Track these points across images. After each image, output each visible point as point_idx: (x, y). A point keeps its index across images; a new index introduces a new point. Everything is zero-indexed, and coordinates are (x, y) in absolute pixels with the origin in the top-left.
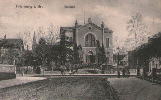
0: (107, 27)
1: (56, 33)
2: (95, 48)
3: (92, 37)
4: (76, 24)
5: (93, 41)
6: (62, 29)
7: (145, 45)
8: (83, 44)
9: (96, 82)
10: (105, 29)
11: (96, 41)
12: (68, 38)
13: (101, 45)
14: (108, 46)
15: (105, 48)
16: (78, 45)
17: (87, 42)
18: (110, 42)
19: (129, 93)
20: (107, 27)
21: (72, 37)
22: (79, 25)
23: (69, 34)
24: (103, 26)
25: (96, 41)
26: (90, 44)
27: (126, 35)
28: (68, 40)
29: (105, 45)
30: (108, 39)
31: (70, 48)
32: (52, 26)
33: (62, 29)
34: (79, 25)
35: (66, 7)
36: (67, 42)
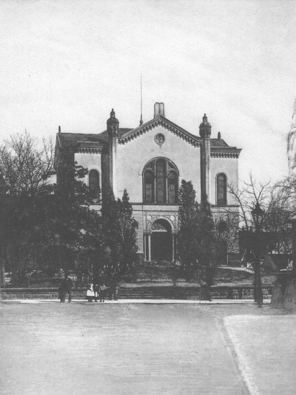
1: (44, 149)
2: (176, 208)
3: (168, 169)
4: (112, 122)
9: (187, 377)
10: (213, 141)
11: (180, 184)
12: (83, 172)
13: (198, 199)
14: (222, 202)
15: (213, 210)
16: (118, 195)
17: (148, 186)
18: (228, 189)
19: (128, 357)
21: (99, 169)
23: (88, 160)
24: (205, 128)
25: (180, 184)
26: (161, 193)
28: (86, 180)
29: (212, 199)
30: (221, 178)
31: (91, 207)
35: (60, 127)
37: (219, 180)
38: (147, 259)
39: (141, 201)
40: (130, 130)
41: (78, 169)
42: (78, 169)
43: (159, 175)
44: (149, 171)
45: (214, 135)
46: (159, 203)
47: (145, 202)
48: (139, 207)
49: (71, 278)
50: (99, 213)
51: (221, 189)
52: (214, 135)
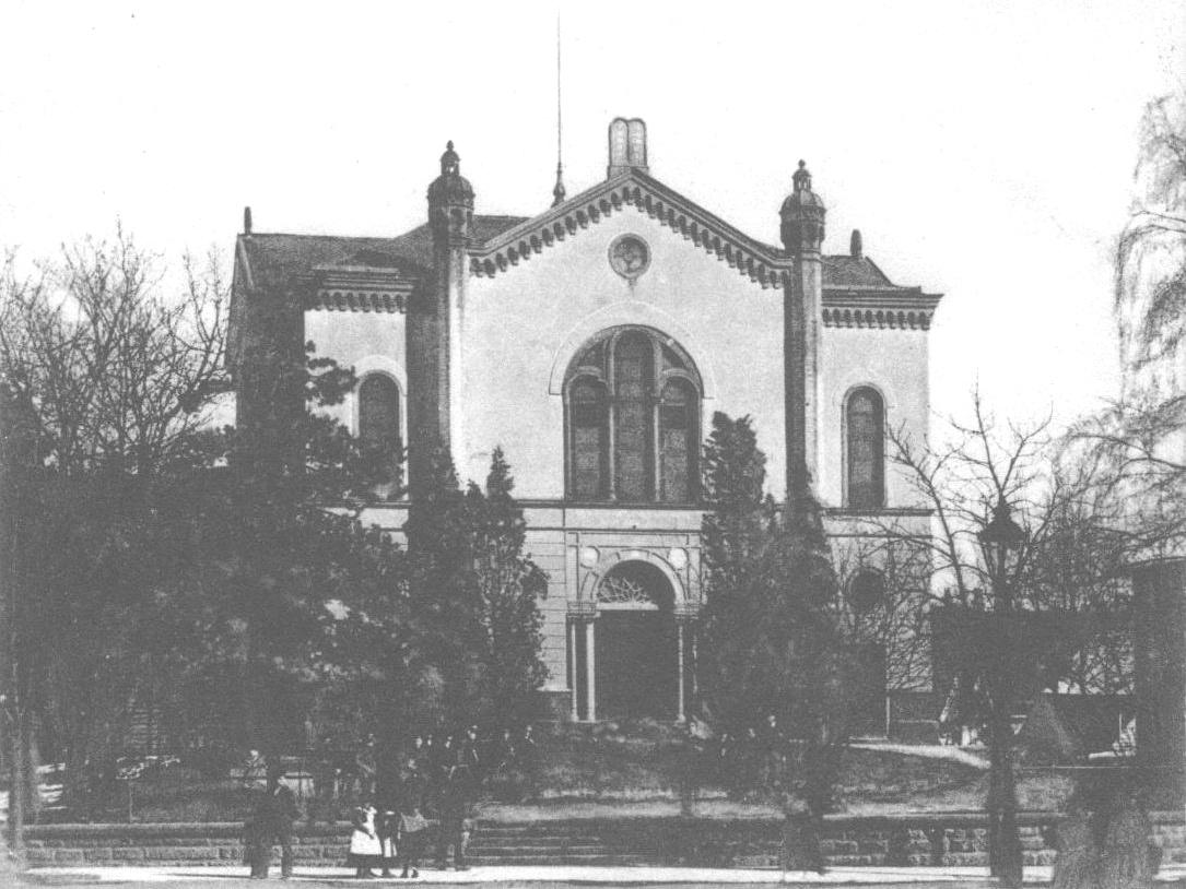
0: (856, 238)
2: (691, 519)
3: (662, 370)
5: (666, 426)
6: (256, 250)
7: (238, 406)
8: (540, 473)
12: (336, 383)
13: (775, 484)
14: (866, 496)
15: (831, 526)
16: (470, 470)
17: (587, 436)
18: (891, 449)
20: (856, 238)
21: (398, 371)
22: (484, 206)
23: (357, 338)
24: (803, 217)
27: (1014, 389)
28: (347, 412)
29: (829, 486)
30: (865, 406)
31: (370, 517)
32: (748, 415)
33: (256, 250)
34: (484, 206)
36: (327, 436)
37: (856, 414)
38: (583, 712)
39: (559, 493)
40: (515, 221)
41: (317, 372)
42: (317, 372)
43: (625, 395)
44: (590, 380)
45: (835, 243)
46: (626, 502)
47: (575, 497)
48: (551, 517)
49: (292, 784)
50: (400, 538)
51: (865, 448)
52: (835, 243)
